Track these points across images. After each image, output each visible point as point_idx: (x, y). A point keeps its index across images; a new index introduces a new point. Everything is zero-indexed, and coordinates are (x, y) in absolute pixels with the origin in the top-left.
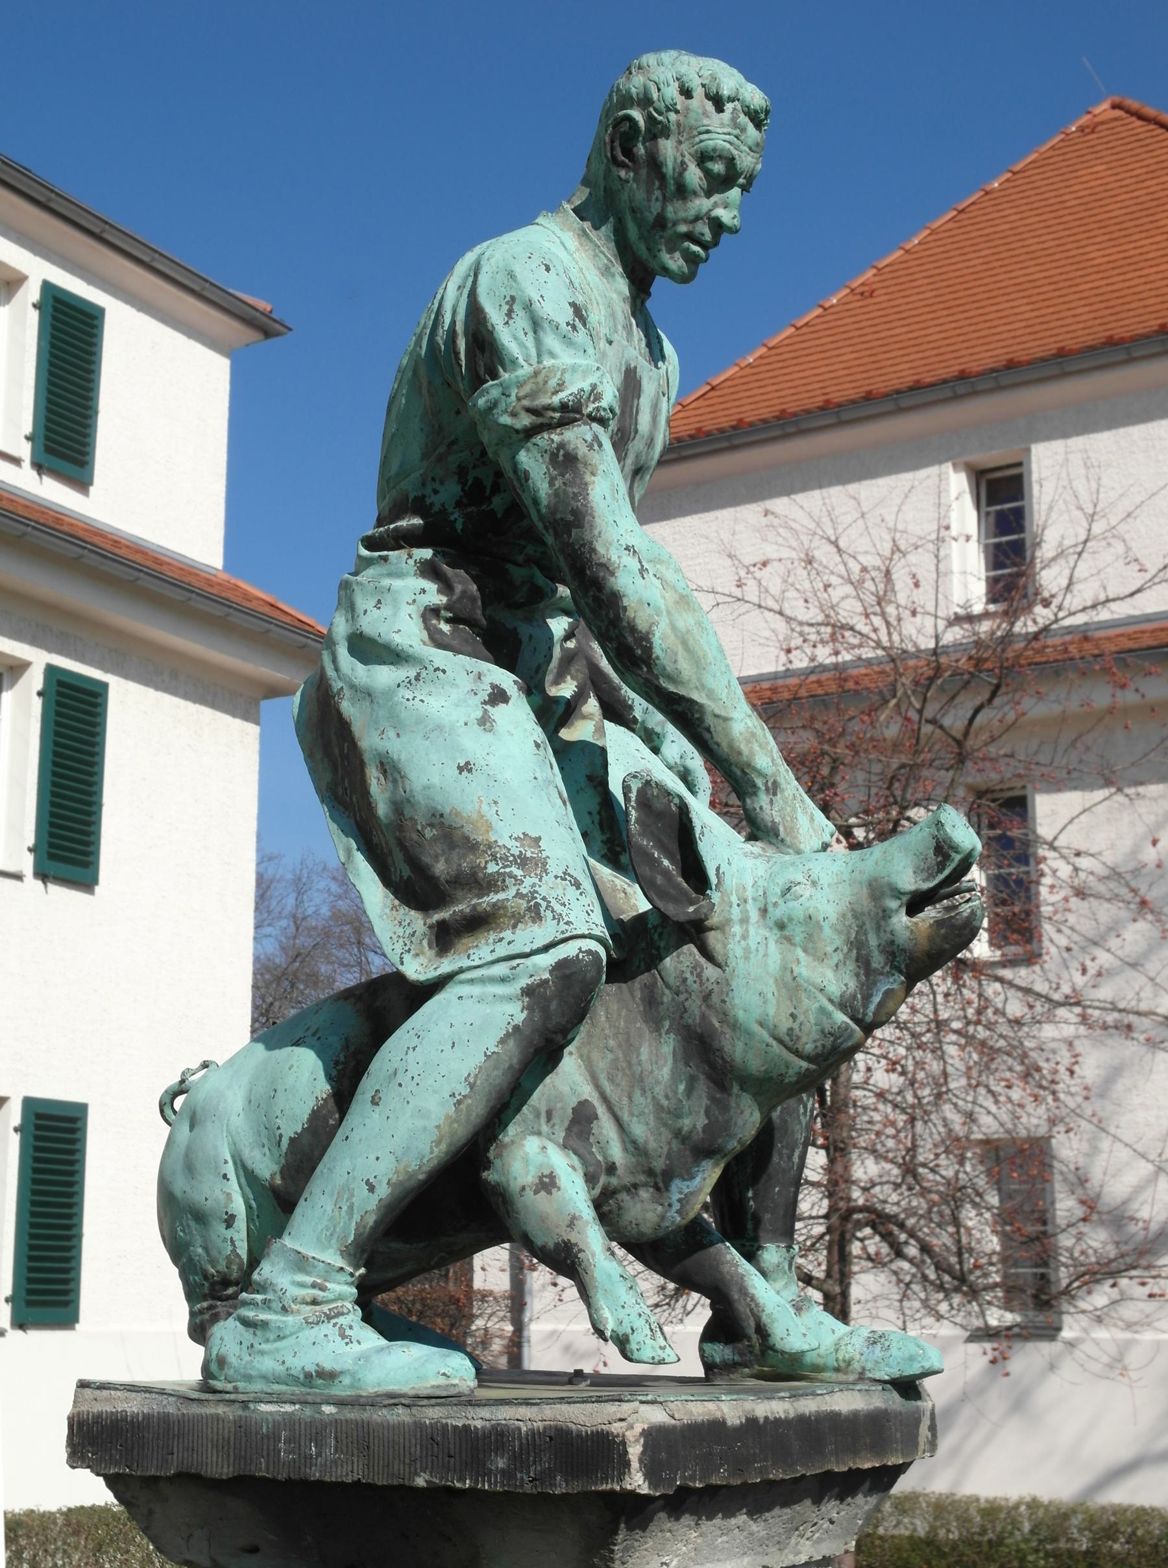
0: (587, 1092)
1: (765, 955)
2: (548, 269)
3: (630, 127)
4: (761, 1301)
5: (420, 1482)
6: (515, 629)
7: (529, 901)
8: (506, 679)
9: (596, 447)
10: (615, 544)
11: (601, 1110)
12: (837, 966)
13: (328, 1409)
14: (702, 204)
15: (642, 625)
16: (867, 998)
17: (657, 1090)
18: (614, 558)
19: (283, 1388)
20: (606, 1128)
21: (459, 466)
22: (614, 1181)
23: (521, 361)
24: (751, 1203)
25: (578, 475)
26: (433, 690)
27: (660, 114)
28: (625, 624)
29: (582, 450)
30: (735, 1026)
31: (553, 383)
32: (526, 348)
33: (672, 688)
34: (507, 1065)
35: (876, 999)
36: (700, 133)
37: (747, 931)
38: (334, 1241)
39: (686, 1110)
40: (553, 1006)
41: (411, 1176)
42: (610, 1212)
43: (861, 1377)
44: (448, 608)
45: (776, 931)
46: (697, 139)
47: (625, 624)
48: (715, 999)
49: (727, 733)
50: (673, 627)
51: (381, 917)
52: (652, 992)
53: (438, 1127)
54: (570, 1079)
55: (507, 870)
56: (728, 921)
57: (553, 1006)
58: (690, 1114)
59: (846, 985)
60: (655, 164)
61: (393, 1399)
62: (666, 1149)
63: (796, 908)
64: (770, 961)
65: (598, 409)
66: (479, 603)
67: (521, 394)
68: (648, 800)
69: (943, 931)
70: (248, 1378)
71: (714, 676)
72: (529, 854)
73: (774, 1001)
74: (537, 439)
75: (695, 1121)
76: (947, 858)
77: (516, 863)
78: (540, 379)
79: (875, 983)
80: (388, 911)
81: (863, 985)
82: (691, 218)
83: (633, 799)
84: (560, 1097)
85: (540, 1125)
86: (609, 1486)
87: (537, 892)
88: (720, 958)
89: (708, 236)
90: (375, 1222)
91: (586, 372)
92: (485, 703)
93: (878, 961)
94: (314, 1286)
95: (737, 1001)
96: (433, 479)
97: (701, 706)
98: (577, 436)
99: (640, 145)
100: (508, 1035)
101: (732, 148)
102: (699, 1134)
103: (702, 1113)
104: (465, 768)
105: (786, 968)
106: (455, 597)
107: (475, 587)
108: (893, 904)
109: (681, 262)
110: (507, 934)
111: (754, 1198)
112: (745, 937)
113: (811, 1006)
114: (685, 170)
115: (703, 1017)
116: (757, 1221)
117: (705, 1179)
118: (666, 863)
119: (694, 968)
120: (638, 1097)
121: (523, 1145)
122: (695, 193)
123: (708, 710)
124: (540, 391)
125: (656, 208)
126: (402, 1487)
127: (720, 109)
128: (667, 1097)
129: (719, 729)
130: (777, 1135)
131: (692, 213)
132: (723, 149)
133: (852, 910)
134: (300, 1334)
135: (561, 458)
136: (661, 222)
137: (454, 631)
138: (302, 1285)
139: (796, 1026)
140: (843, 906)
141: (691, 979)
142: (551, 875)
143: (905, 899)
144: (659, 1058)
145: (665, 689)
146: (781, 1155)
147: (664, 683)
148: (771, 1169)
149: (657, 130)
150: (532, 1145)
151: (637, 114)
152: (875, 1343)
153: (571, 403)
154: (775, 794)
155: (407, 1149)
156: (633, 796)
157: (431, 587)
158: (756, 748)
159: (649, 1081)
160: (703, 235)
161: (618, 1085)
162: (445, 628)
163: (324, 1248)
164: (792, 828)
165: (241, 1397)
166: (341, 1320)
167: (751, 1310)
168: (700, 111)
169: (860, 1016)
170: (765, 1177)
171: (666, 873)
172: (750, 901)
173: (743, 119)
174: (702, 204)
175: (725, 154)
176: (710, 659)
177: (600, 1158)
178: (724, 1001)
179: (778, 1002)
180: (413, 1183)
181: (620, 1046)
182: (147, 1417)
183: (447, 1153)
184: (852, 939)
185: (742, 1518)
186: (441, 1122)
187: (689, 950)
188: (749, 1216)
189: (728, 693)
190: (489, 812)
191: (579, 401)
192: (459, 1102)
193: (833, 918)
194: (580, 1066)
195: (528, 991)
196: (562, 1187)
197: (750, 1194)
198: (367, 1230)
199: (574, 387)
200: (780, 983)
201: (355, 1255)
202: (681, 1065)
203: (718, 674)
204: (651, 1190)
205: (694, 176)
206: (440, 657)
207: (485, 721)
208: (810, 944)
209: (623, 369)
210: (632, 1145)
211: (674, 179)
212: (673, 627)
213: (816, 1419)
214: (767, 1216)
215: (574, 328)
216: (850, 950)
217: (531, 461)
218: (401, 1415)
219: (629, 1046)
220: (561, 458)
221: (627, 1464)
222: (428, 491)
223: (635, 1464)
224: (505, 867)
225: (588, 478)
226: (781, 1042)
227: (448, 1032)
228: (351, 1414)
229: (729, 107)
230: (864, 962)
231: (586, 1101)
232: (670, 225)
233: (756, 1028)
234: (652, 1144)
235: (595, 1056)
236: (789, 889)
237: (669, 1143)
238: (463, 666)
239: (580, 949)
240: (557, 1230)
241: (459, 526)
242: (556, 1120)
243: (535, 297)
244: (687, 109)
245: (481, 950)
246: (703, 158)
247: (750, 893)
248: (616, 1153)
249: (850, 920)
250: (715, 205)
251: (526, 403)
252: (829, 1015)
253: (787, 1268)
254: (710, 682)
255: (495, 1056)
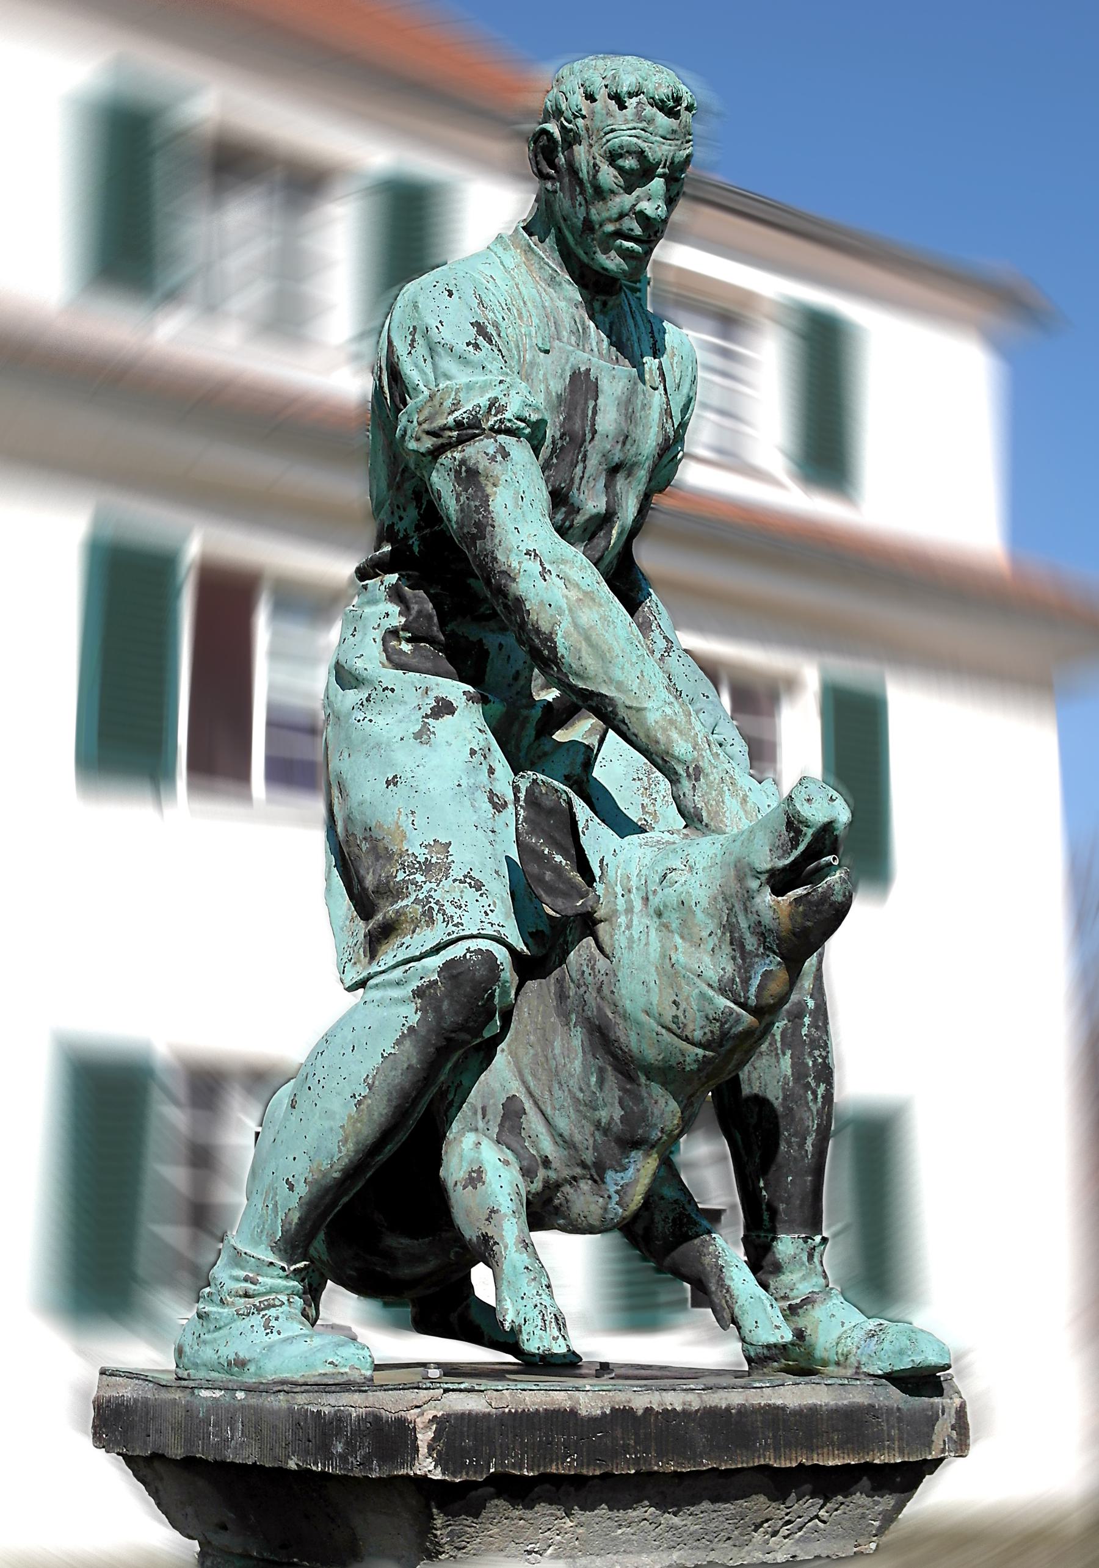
0: (515, 1088)
1: (647, 944)
2: (450, 294)
3: (549, 140)
4: (735, 1293)
5: (292, 1465)
6: (481, 640)
7: (424, 906)
8: (455, 690)
9: (499, 458)
10: (515, 551)
11: (528, 1105)
12: (713, 950)
13: (240, 1395)
14: (625, 201)
15: (545, 627)
16: (746, 981)
17: (571, 1083)
18: (515, 564)
19: (214, 1375)
20: (533, 1122)
21: (414, 491)
22: (553, 1175)
23: (422, 387)
24: (764, 1193)
25: (480, 488)
26: (382, 707)
27: (570, 122)
28: (530, 627)
29: (483, 464)
30: (625, 1017)
31: (448, 403)
32: (425, 374)
33: (581, 685)
34: (406, 1066)
35: (755, 982)
36: (606, 134)
37: (631, 920)
38: (264, 1238)
39: (600, 1102)
40: (445, 1006)
41: (324, 1175)
42: (561, 1204)
43: (858, 1374)
44: (405, 628)
45: (655, 919)
46: (604, 140)
47: (530, 627)
48: (606, 991)
49: (642, 722)
50: (576, 625)
51: (342, 929)
52: (562, 987)
53: (342, 1127)
54: (501, 1076)
55: (411, 877)
56: (615, 913)
57: (445, 1006)
58: (605, 1105)
59: (723, 969)
60: (573, 169)
61: (288, 1386)
62: (591, 1141)
63: (669, 895)
64: (651, 950)
65: (501, 421)
66: (436, 620)
67: (421, 419)
68: (536, 798)
69: (801, 908)
70: (196, 1366)
71: (623, 668)
72: (434, 860)
73: (657, 990)
74: (442, 459)
75: (611, 1113)
76: (799, 832)
77: (421, 869)
78: (436, 401)
79: (752, 965)
80: (348, 923)
81: (740, 968)
82: (615, 216)
83: (522, 799)
84: (492, 1093)
85: (477, 1121)
86: (465, 1477)
87: (431, 897)
88: (608, 950)
89: (638, 231)
90: (299, 1218)
91: (484, 387)
92: (427, 716)
93: (751, 943)
94: (246, 1279)
95: (623, 992)
96: (398, 507)
97: (611, 699)
98: (478, 451)
99: (561, 155)
100: (403, 1036)
101: (639, 142)
102: (618, 1126)
103: (617, 1104)
104: (392, 782)
105: (665, 956)
106: (411, 618)
107: (431, 605)
108: (754, 884)
109: (619, 260)
110: (407, 940)
111: (765, 1188)
112: (629, 927)
113: (691, 992)
114: (598, 171)
115: (599, 1008)
116: (773, 1212)
117: (638, 1170)
118: (558, 858)
119: (589, 960)
120: (558, 1093)
121: (461, 1142)
122: (612, 192)
123: (619, 702)
124: (436, 413)
125: (581, 213)
126: (280, 1468)
127: (622, 106)
128: (581, 1090)
129: (634, 720)
130: (782, 1123)
131: (614, 212)
132: (630, 144)
133: (723, 893)
134: (233, 1325)
135: (464, 474)
136: (588, 226)
137: (414, 651)
138: (237, 1279)
139: (680, 1013)
140: (715, 889)
141: (587, 971)
142: (450, 879)
143: (764, 877)
144: (571, 1050)
145: (575, 686)
146: (789, 1144)
147: (574, 681)
148: (779, 1158)
149: (571, 139)
150: (470, 1139)
151: (553, 127)
152: (873, 1336)
153: (465, 421)
154: (697, 779)
155: (318, 1149)
156: (522, 796)
157: (394, 609)
158: (675, 735)
159: (564, 1075)
160: (632, 230)
161: (539, 1080)
162: (406, 647)
163: (256, 1244)
164: (717, 813)
165: (191, 1384)
166: (272, 1312)
167: (727, 1302)
168: (604, 112)
169: (742, 1000)
170: (774, 1168)
171: (557, 869)
172: (634, 890)
173: (650, 111)
174: (625, 201)
175: (633, 148)
176: (617, 650)
177: (534, 1153)
178: (613, 992)
179: (660, 990)
180: (328, 1180)
181: (538, 1040)
182: (136, 1401)
183: (356, 1152)
184: (724, 923)
185: (603, 1510)
186: (345, 1122)
187: (587, 943)
188: (764, 1207)
189: (641, 683)
190: (405, 822)
191: (475, 417)
192: (359, 1103)
193: (705, 903)
194: (509, 1063)
195: (418, 993)
196: (487, 1181)
197: (762, 1184)
198: (293, 1226)
199: (473, 402)
200: (660, 970)
201: (285, 1251)
202: (589, 1056)
203: (627, 665)
204: (590, 1182)
205: (608, 175)
206: (391, 676)
207: (423, 735)
208: (686, 930)
209: (568, 374)
210: (563, 1141)
211: (590, 182)
212: (576, 625)
213: (739, 1412)
214: (782, 1207)
215: (477, 346)
216: (724, 933)
217: (441, 481)
218: (280, 1402)
219: (546, 1041)
220: (464, 474)
221: (416, 1450)
222: (396, 519)
223: (423, 1450)
224: (411, 874)
225: (489, 490)
226: (669, 1030)
227: (350, 1036)
228: (254, 1400)
229: (631, 103)
230: (737, 943)
231: (514, 1096)
232: (597, 227)
233: (644, 1018)
234: (578, 1138)
235: (521, 1051)
236: (665, 876)
237: (593, 1135)
238: (413, 682)
239: (468, 950)
240: (478, 1224)
241: (416, 549)
242: (489, 1116)
243: (433, 323)
244: (593, 113)
245: (389, 955)
246: (613, 157)
247: (634, 883)
248: (548, 1146)
249: (721, 904)
250: (639, 199)
251: (425, 426)
252: (710, 1001)
253: (805, 1258)
254: (618, 675)
255: (391, 1057)
